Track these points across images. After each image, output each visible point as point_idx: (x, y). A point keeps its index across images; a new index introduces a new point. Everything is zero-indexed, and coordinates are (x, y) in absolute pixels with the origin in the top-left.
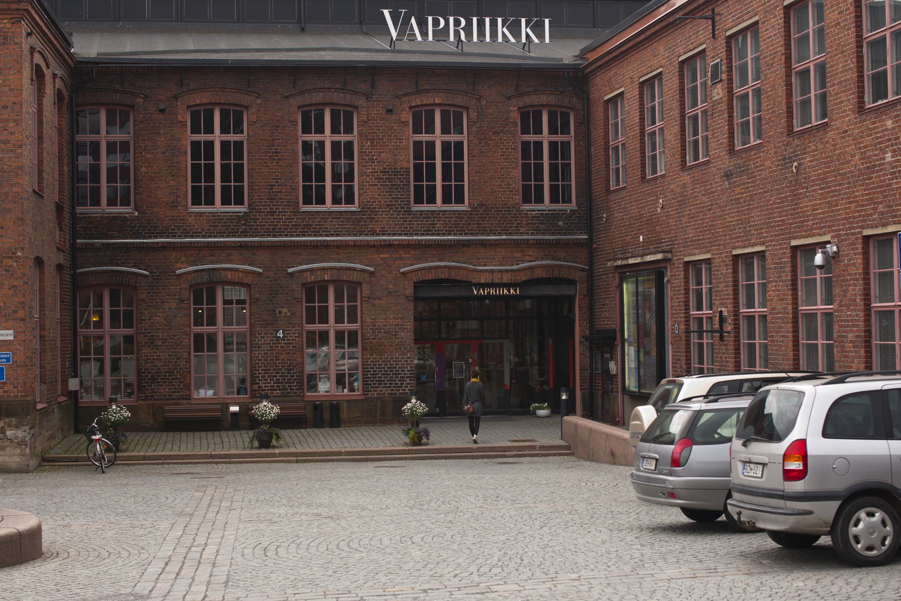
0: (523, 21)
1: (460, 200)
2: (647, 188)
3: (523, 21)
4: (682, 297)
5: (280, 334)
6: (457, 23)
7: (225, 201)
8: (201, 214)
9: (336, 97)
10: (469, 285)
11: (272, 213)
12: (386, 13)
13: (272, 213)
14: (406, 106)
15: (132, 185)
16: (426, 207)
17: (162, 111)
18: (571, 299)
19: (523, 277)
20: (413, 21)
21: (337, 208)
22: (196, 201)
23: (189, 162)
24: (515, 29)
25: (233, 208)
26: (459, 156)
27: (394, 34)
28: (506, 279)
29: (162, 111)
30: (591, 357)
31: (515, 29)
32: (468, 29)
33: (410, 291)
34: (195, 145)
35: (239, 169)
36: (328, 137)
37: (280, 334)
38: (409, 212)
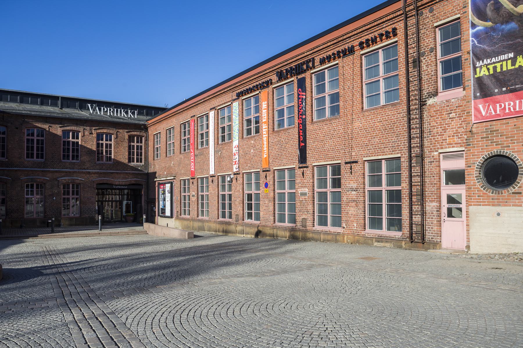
0: (129, 111)
1: (141, 162)
2: (167, 159)
3: (129, 111)
4: (179, 189)
5: (54, 198)
6: (110, 110)
7: (137, 161)
8: (29, 161)
9: (138, 133)
10: (113, 185)
11: (53, 162)
12: (89, 105)
13: (53, 162)
14: (96, 132)
15: (6, 151)
16: (100, 162)
17: (17, 128)
18: (140, 191)
19: (128, 183)
20: (97, 108)
21: (138, 163)
22: (28, 157)
23: (26, 145)
24: (127, 113)
25: (40, 160)
26: (141, 149)
27: (91, 111)
28: (123, 183)
29: (17, 128)
30: (148, 206)
31: (127, 113)
32: (113, 112)
33: (95, 186)
34: (28, 140)
35: (42, 148)
36: (35, 138)
37: (54, 198)
38: (95, 163)
